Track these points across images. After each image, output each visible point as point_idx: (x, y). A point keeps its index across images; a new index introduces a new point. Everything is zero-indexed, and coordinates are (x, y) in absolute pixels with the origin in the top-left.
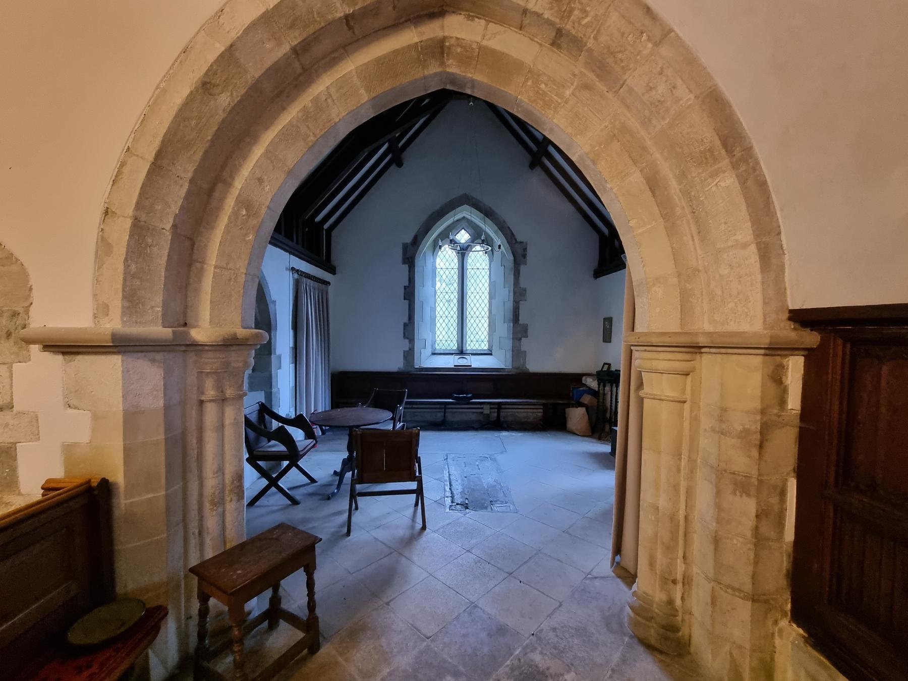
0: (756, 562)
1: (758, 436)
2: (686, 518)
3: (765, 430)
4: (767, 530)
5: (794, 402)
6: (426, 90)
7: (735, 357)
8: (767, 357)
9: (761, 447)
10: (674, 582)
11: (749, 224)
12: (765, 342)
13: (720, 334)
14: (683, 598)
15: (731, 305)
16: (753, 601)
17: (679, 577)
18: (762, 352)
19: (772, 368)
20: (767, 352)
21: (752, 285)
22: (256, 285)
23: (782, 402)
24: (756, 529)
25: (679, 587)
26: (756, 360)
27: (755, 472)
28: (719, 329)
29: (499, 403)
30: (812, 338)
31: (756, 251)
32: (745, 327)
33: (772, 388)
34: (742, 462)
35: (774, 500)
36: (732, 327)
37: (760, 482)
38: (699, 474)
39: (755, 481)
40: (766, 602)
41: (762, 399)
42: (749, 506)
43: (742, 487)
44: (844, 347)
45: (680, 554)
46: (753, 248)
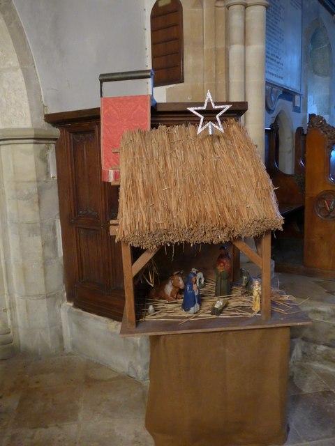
0: (45, 274)
1: (37, 196)
2: (6, 263)
3: (40, 191)
4: (49, 254)
5: (53, 173)
6: (81, 314)
7: (20, 146)
8: (36, 145)
9: (39, 202)
10: (5, 310)
11: (16, 54)
12: (32, 134)
13: (8, 130)
14: (11, 319)
15: (12, 110)
16: (47, 297)
17: (7, 306)
18: (32, 141)
19: (39, 152)
20: (35, 141)
21: (22, 97)
22: (135, 264)
23: (48, 173)
24: (43, 253)
25: (8, 312)
26: (30, 147)
27: (38, 219)
28: (8, 126)
29: (55, 242)
30: (56, 132)
31: (22, 74)
32: (22, 125)
33: (42, 165)
34: (30, 214)
35: (50, 234)
36: (15, 125)
37: (42, 224)
38: (10, 231)
39: (39, 225)
40: (54, 296)
41: (36, 171)
42: (38, 241)
43: (33, 231)
44: (70, 136)
45: (6, 292)
46: (20, 70)
